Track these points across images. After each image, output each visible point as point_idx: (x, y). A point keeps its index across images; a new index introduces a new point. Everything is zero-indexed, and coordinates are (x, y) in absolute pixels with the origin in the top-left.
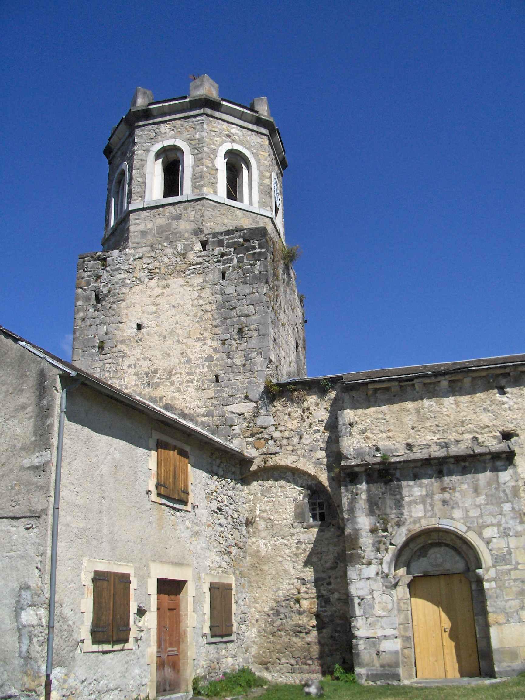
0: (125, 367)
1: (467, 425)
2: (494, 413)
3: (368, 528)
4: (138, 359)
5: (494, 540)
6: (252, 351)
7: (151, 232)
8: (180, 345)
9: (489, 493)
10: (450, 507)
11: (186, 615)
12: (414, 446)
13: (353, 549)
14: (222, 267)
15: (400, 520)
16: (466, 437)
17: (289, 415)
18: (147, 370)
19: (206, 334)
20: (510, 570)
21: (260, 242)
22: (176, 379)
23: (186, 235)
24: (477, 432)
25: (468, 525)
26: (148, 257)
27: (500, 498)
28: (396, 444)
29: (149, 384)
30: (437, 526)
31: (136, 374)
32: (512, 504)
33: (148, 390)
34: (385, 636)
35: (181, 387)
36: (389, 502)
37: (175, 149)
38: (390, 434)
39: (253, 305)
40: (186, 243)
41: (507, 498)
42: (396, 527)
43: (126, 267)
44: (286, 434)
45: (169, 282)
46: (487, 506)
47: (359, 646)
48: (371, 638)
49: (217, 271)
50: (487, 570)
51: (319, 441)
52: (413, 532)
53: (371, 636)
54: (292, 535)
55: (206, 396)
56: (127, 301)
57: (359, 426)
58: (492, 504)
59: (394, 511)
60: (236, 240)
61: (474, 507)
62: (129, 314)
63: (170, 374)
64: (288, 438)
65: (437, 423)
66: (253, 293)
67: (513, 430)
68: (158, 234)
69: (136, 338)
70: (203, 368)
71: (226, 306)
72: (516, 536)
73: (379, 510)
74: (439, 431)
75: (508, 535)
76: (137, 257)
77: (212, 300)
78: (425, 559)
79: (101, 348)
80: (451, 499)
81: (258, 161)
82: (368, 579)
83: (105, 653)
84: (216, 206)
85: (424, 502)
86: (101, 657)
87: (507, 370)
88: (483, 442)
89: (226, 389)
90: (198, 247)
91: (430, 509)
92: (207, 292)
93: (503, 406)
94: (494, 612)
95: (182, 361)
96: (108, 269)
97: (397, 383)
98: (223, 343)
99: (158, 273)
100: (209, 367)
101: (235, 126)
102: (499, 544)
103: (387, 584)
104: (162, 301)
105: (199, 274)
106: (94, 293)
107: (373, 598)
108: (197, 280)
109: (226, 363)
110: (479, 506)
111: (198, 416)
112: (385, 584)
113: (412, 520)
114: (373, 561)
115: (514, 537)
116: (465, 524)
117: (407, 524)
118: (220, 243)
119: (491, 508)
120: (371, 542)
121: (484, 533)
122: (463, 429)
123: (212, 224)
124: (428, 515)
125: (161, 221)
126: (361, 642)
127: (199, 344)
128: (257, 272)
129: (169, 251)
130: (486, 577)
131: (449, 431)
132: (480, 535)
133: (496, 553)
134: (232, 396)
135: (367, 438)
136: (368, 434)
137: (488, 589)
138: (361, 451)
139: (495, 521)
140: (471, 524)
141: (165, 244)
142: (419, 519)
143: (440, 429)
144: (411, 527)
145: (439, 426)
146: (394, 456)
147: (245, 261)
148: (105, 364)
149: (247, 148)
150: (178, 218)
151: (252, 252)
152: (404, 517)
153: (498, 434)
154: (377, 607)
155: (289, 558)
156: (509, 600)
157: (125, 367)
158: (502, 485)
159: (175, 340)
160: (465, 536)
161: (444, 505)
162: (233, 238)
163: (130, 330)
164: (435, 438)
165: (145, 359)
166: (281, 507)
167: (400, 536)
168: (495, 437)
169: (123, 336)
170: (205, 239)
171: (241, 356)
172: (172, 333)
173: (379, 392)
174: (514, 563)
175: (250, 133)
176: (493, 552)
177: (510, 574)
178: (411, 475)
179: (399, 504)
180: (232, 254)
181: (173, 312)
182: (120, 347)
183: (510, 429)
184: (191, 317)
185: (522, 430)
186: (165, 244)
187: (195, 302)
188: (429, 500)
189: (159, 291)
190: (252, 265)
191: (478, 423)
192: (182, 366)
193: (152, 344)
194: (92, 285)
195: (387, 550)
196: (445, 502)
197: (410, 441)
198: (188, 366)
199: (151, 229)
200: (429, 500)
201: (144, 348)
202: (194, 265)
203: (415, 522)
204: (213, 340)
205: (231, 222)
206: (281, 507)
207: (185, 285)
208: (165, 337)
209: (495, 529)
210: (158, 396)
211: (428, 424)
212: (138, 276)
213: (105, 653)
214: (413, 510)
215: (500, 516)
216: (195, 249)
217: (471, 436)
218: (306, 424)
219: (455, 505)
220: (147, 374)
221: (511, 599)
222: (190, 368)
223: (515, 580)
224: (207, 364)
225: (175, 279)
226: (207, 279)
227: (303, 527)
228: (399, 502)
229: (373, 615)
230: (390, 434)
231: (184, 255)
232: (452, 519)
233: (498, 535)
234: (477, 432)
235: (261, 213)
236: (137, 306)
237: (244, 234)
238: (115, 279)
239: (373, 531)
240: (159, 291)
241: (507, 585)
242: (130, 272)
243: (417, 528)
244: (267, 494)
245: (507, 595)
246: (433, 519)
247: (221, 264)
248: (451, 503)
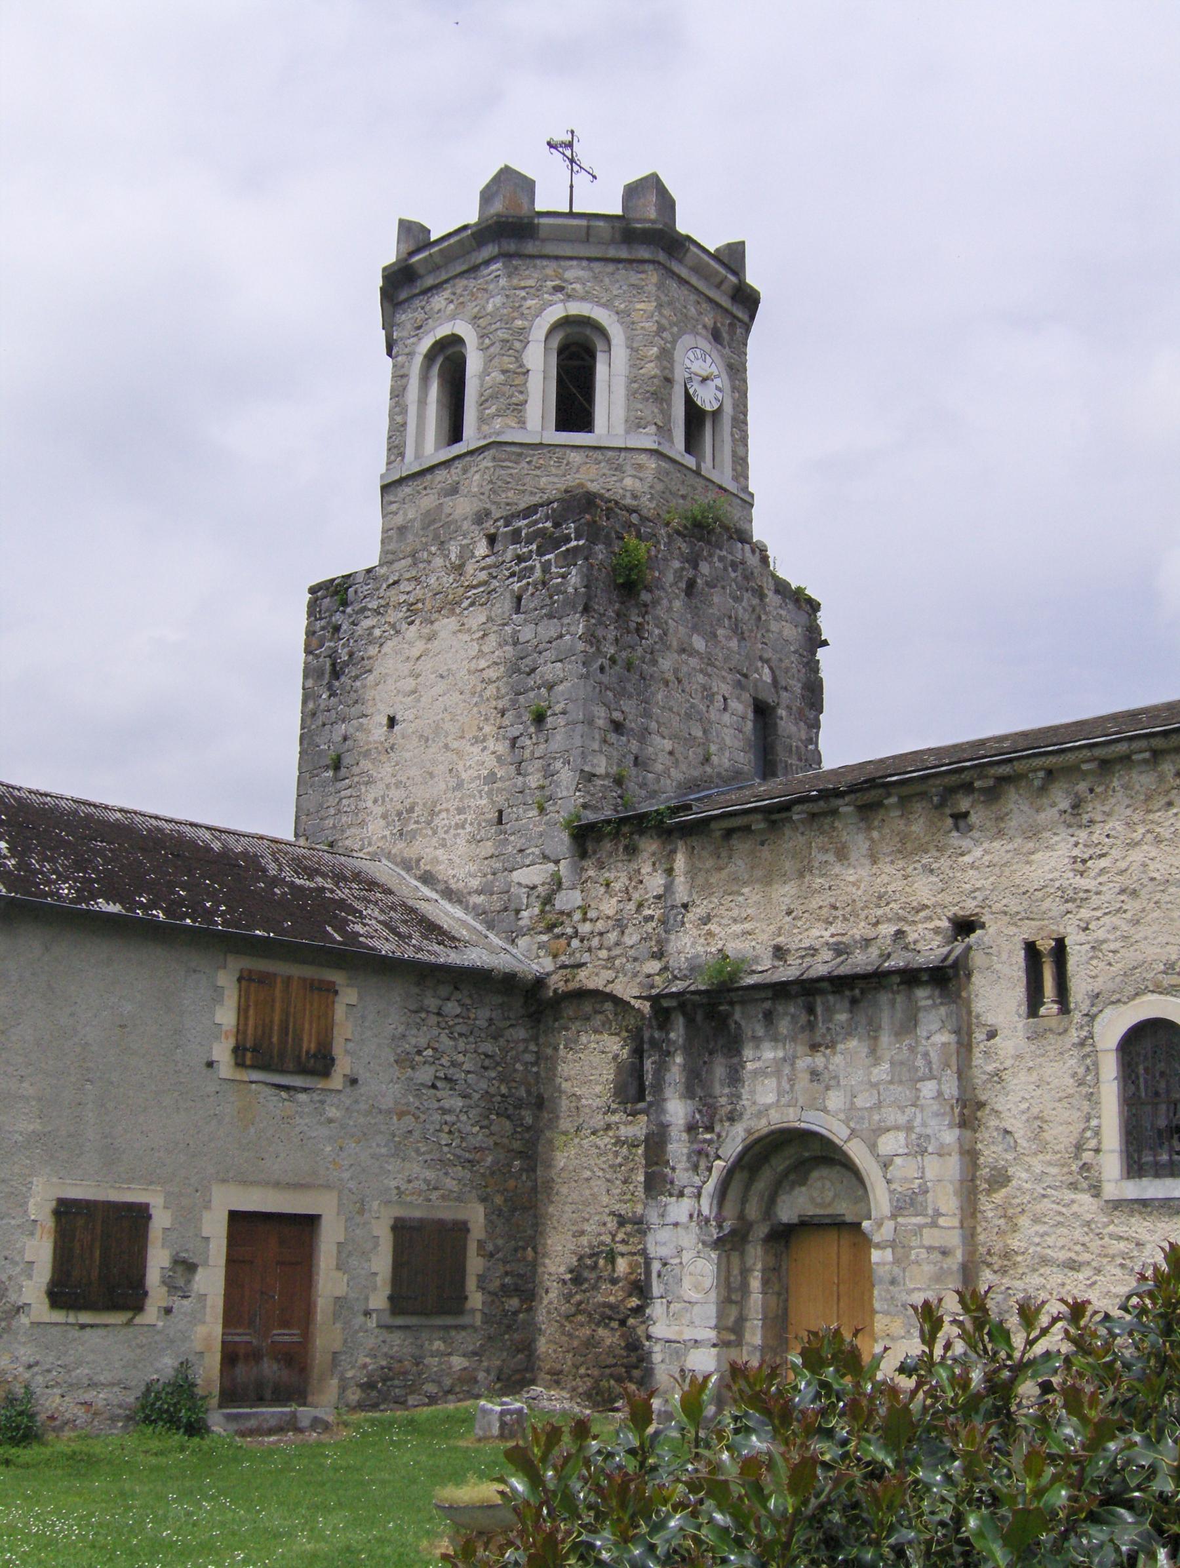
0: (369, 804)
1: (888, 904)
2: (941, 876)
3: (681, 1122)
4: (388, 786)
5: (898, 1161)
6: (555, 758)
7: (413, 526)
8: (449, 754)
9: (896, 1057)
10: (823, 1085)
11: (318, 1274)
12: (788, 950)
13: (657, 1164)
14: (516, 586)
15: (735, 1109)
16: (883, 932)
17: (608, 885)
18: (399, 807)
19: (487, 729)
20: (921, 1227)
21: (577, 524)
22: (441, 821)
23: (466, 525)
24: (904, 919)
25: (852, 1125)
26: (408, 580)
27: (917, 1069)
28: (758, 947)
29: (401, 835)
30: (797, 1124)
31: (384, 816)
32: (939, 1084)
33: (401, 845)
34: (696, 1341)
35: (446, 836)
36: (720, 1071)
37: (455, 341)
38: (747, 926)
39: (560, 661)
40: (465, 542)
41: (931, 1069)
42: (727, 1124)
43: (373, 605)
44: (600, 926)
45: (436, 626)
46: (892, 1087)
47: (654, 1356)
48: (674, 1342)
49: (508, 595)
50: (880, 1225)
51: (651, 939)
52: (756, 1135)
53: (673, 1337)
54: (608, 1127)
55: (484, 854)
56: (375, 673)
57: (698, 910)
58: (901, 1082)
59: (727, 1091)
60: (541, 525)
61: (867, 1087)
62: (377, 697)
63: (433, 813)
64: (601, 934)
65: (832, 900)
66: (561, 636)
67: (977, 914)
68: (423, 529)
69: (387, 745)
70: (481, 797)
71: (520, 667)
72: (940, 1155)
73: (703, 1089)
74: (836, 918)
75: (923, 1152)
76: (391, 581)
77: (499, 657)
78: (803, 1189)
79: (337, 765)
80: (826, 1068)
81: (630, 328)
82: (676, 1225)
83: (83, 1327)
84: (520, 455)
85: (778, 1073)
86: (75, 1333)
87: (966, 777)
88: (915, 942)
89: (512, 838)
90: (482, 549)
91: (787, 1087)
92: (492, 640)
93: (960, 859)
94: (887, 1313)
95: (450, 785)
96: (349, 610)
97: (759, 817)
98: (513, 746)
99: (421, 610)
100: (490, 793)
101: (575, 263)
102: (904, 1168)
103: (706, 1238)
104: (425, 665)
105: (482, 605)
106: (328, 662)
107: (681, 1263)
108: (477, 618)
109: (515, 785)
110: (875, 1085)
111: (469, 893)
112: (703, 1237)
113: (754, 1109)
114: (686, 1191)
115: (935, 1156)
116: (846, 1122)
117: (746, 1117)
118: (515, 537)
119: (900, 1092)
120: (685, 1151)
121: (879, 1144)
122: (880, 912)
123: (510, 494)
124: (783, 1101)
125: (428, 501)
126: (657, 1348)
127: (476, 750)
128: (570, 590)
129: (438, 562)
130: (876, 1239)
131: (852, 919)
132: (873, 1147)
133: (900, 1189)
134: (521, 851)
135: (710, 934)
136: (713, 927)
137: (878, 1264)
138: (699, 961)
139: (902, 1119)
140: (858, 1123)
141: (433, 549)
142: (767, 1108)
143: (839, 913)
144: (752, 1123)
145: (836, 908)
146: (754, 972)
147: (554, 570)
148: (341, 799)
149: (604, 306)
150: (454, 490)
151: (564, 548)
152: (741, 1103)
153: (945, 924)
154: (686, 1284)
155: (601, 1174)
156: (915, 1289)
157: (369, 804)
158: (923, 1042)
159: (441, 744)
160: (845, 1148)
161: (812, 1081)
162: (536, 522)
163: (378, 731)
164: (827, 934)
165: (398, 784)
166: (594, 1072)
167: (734, 1141)
168: (937, 930)
169: (368, 743)
170: (493, 531)
171: (538, 770)
172: (437, 729)
173: (735, 836)
174: (930, 1212)
175: (611, 268)
176: (893, 1186)
177: (921, 1235)
178: (760, 1016)
179: (735, 1078)
180: (534, 557)
181: (441, 686)
182: (365, 764)
183: (968, 913)
184: (467, 696)
185: (993, 913)
186: (433, 549)
187: (473, 665)
188: (787, 1070)
189: (420, 646)
190: (564, 576)
191: (908, 900)
192: (449, 795)
193: (407, 755)
194: (327, 644)
195: (710, 1169)
196: (815, 1074)
197: (781, 940)
198: (458, 794)
199: (412, 521)
200: (787, 1070)
201: (397, 765)
202: (474, 587)
203: (759, 1114)
204: (497, 740)
205: (556, 480)
206: (594, 1072)
207: (460, 631)
208: (427, 740)
209: (902, 1136)
210: (414, 857)
211: (815, 903)
212: (392, 620)
213: (83, 1327)
214: (759, 1088)
215: (913, 1109)
216: (477, 553)
217: (893, 929)
218: (632, 906)
219: (832, 1083)
220: (399, 814)
221: (919, 1289)
222: (461, 799)
223: (930, 1249)
224: (486, 789)
225: (446, 620)
226: (493, 614)
227: (625, 1112)
228: (737, 1071)
229: (680, 1299)
230: (747, 926)
231: (459, 569)
232: (825, 1110)
233: (906, 1151)
234: (904, 919)
235: (629, 445)
236: (390, 681)
237: (554, 510)
238: (359, 630)
239: (691, 1128)
240: (420, 646)
241: (913, 1257)
242: (379, 613)
243: (762, 1126)
244: (572, 1046)
245: (911, 1279)
246: (791, 1110)
247: (516, 579)
248: (826, 1076)
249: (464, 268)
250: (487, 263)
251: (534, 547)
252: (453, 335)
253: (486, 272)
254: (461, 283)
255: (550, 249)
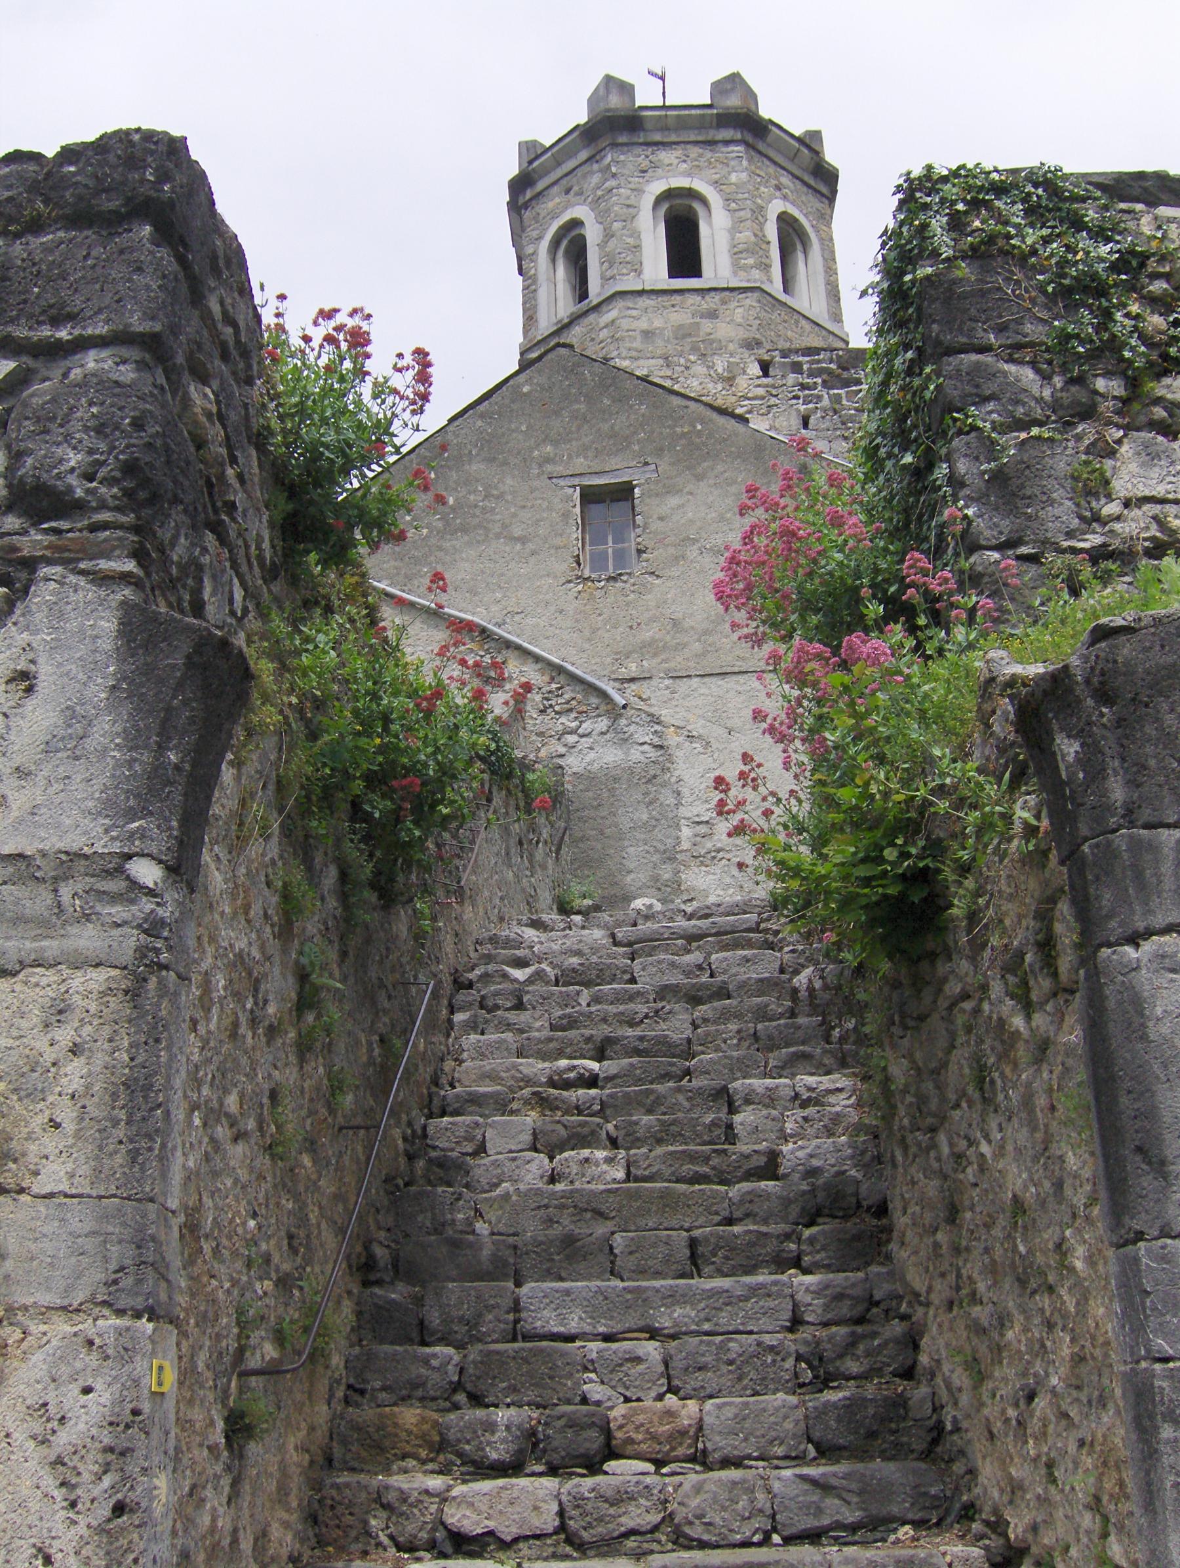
37: (576, 223)
150: (712, 315)
162: (819, 362)
170: (766, 357)
249: (700, 138)
250: (727, 143)
251: (819, 380)
252: (690, 189)
253: (724, 149)
254: (694, 151)
255: (772, 154)
